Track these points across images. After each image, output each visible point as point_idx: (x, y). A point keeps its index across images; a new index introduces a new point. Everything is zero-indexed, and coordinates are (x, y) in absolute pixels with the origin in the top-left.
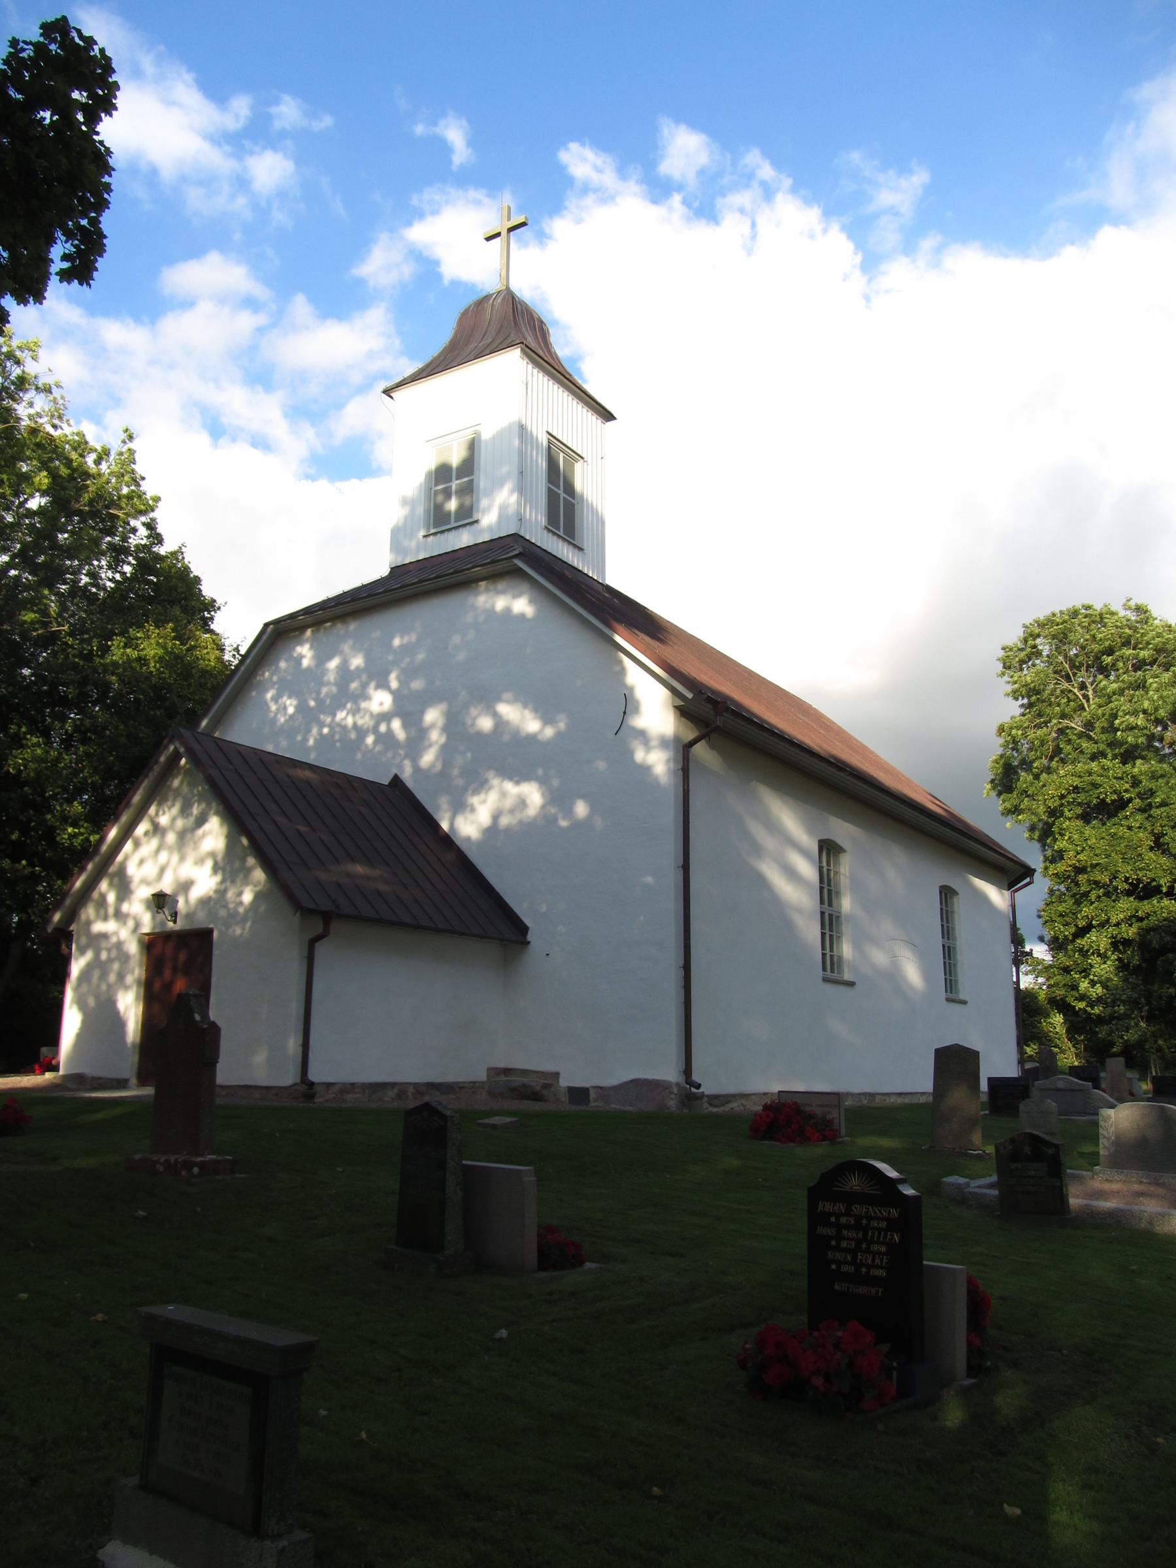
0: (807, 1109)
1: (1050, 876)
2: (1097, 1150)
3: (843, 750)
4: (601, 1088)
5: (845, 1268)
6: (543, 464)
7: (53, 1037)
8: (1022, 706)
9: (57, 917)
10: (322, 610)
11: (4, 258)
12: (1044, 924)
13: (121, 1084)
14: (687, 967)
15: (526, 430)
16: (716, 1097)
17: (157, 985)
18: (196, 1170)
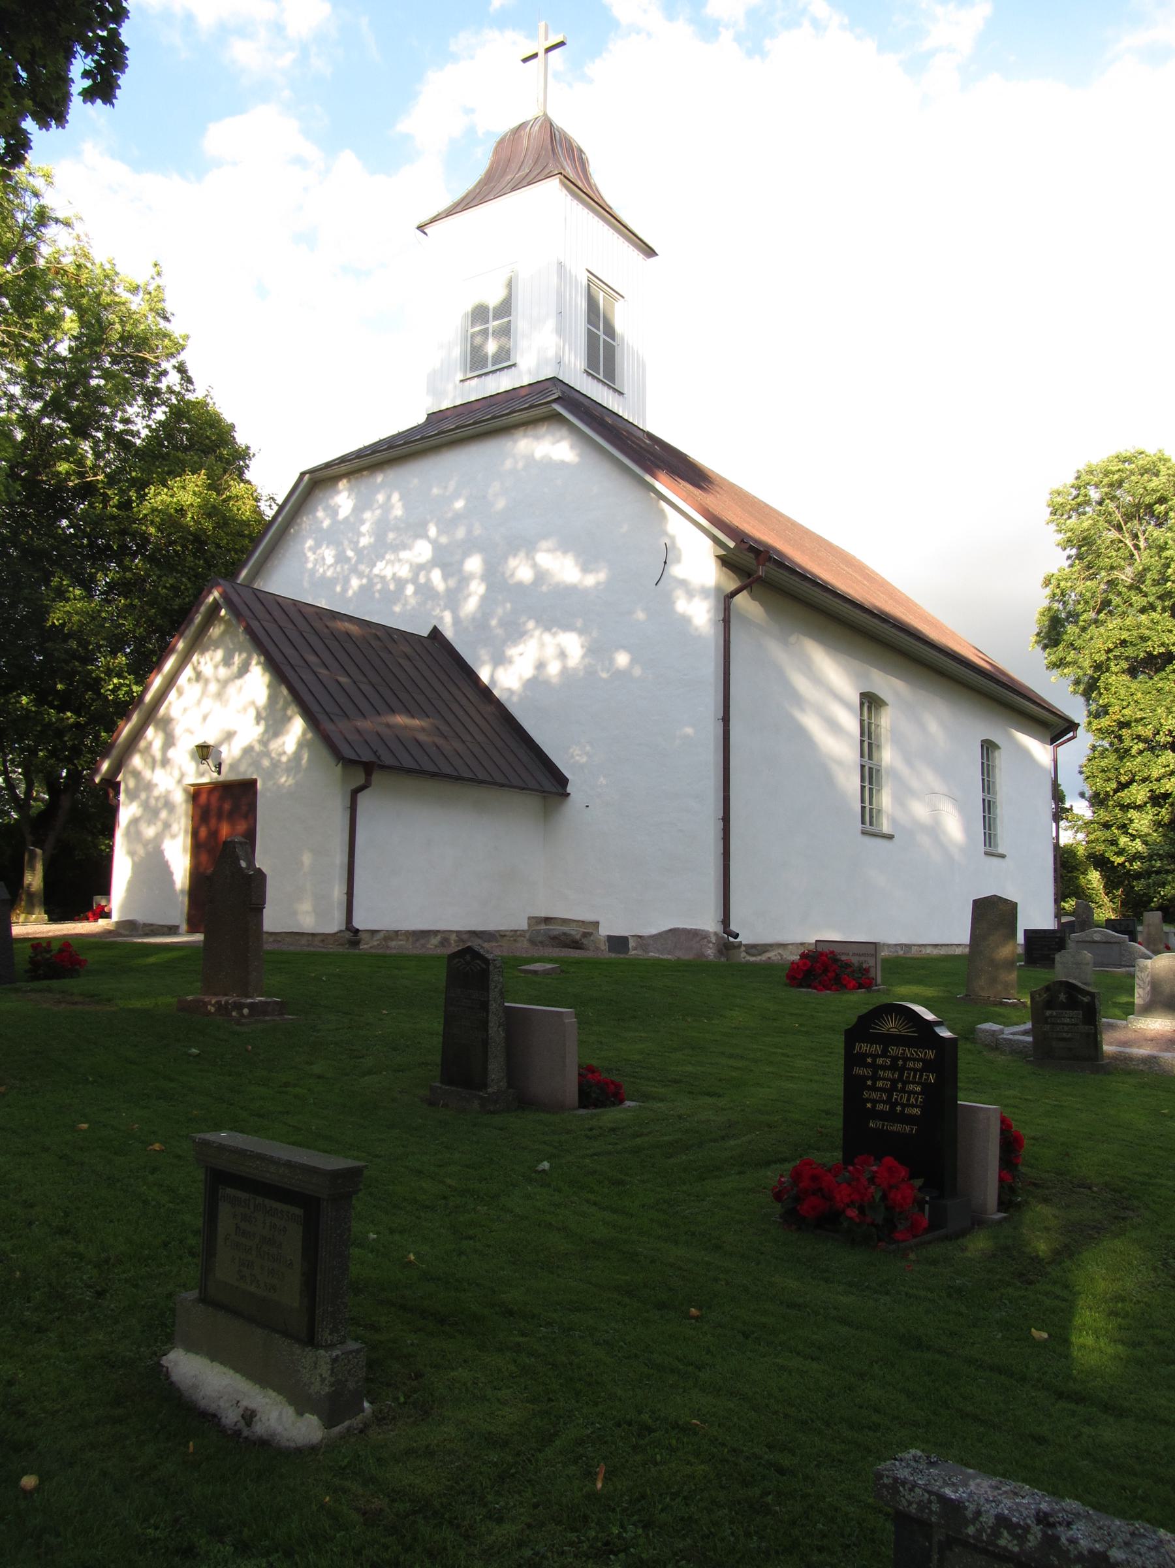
0: (844, 958)
1: (1094, 731)
2: (1132, 1000)
3: (886, 601)
4: (640, 937)
5: (880, 1107)
6: (583, 305)
7: (105, 889)
8: (1069, 557)
9: (105, 766)
10: (359, 458)
11: (23, 78)
12: (1085, 779)
13: (172, 930)
14: (726, 819)
15: (565, 269)
16: (754, 946)
17: (203, 832)
18: (246, 1011)
